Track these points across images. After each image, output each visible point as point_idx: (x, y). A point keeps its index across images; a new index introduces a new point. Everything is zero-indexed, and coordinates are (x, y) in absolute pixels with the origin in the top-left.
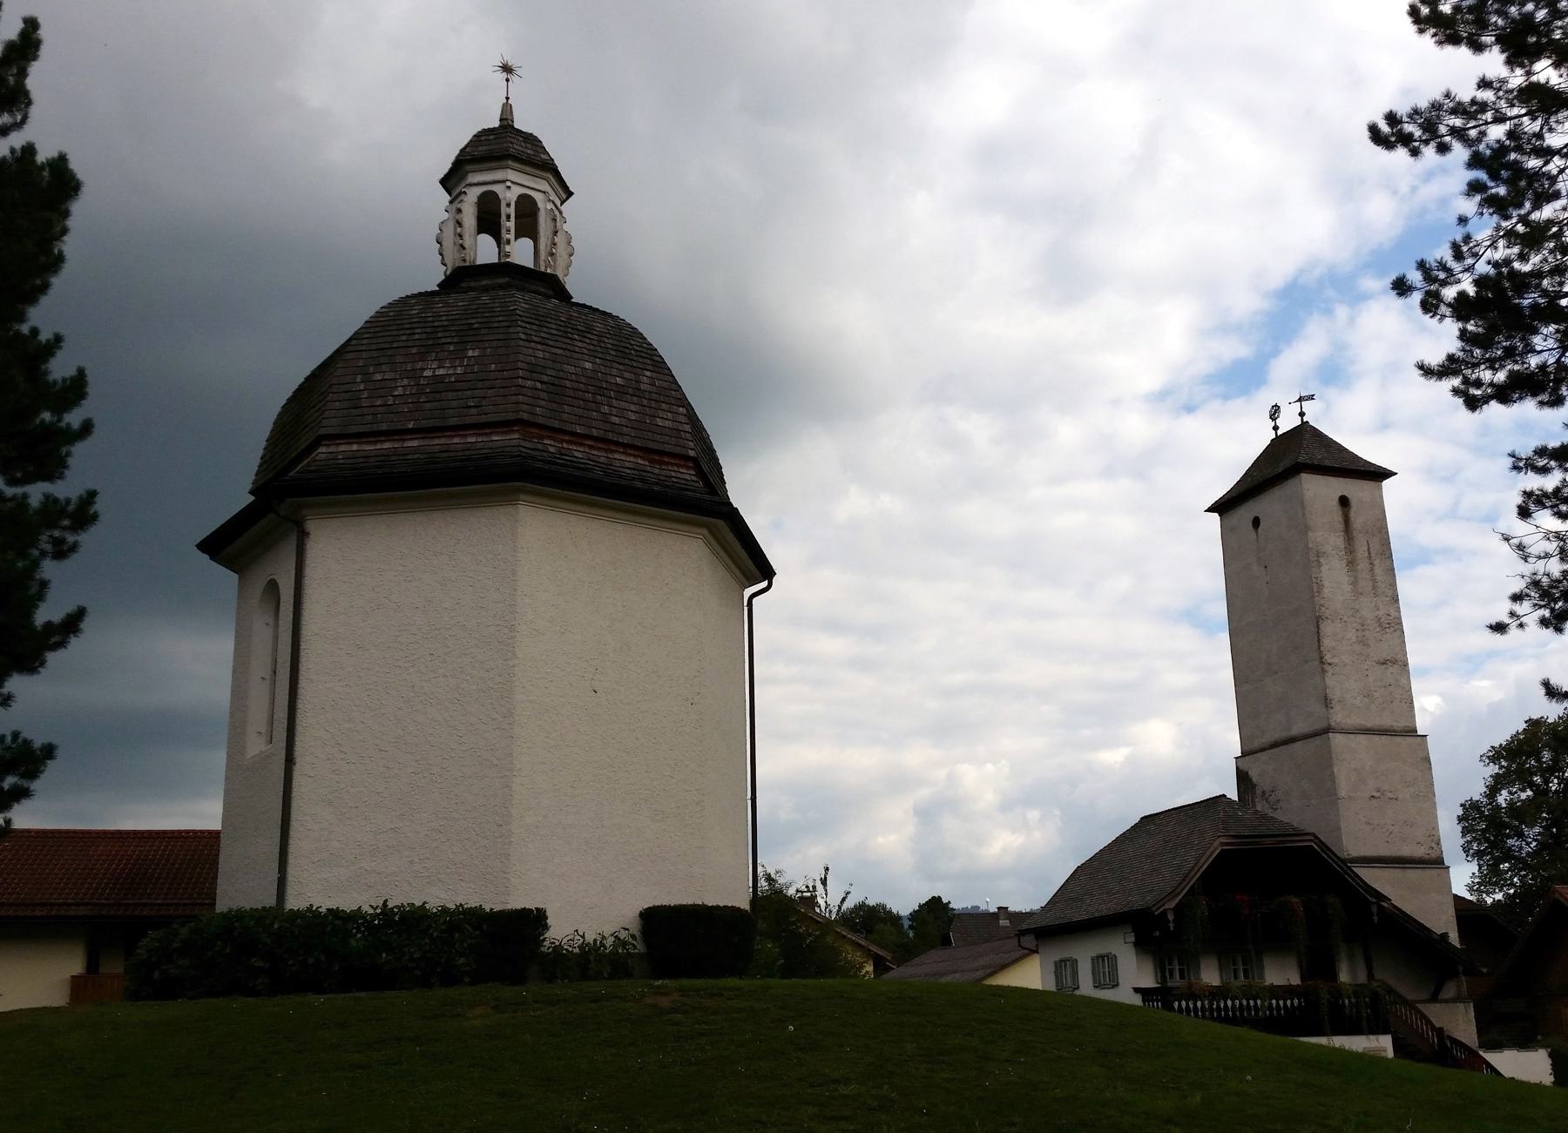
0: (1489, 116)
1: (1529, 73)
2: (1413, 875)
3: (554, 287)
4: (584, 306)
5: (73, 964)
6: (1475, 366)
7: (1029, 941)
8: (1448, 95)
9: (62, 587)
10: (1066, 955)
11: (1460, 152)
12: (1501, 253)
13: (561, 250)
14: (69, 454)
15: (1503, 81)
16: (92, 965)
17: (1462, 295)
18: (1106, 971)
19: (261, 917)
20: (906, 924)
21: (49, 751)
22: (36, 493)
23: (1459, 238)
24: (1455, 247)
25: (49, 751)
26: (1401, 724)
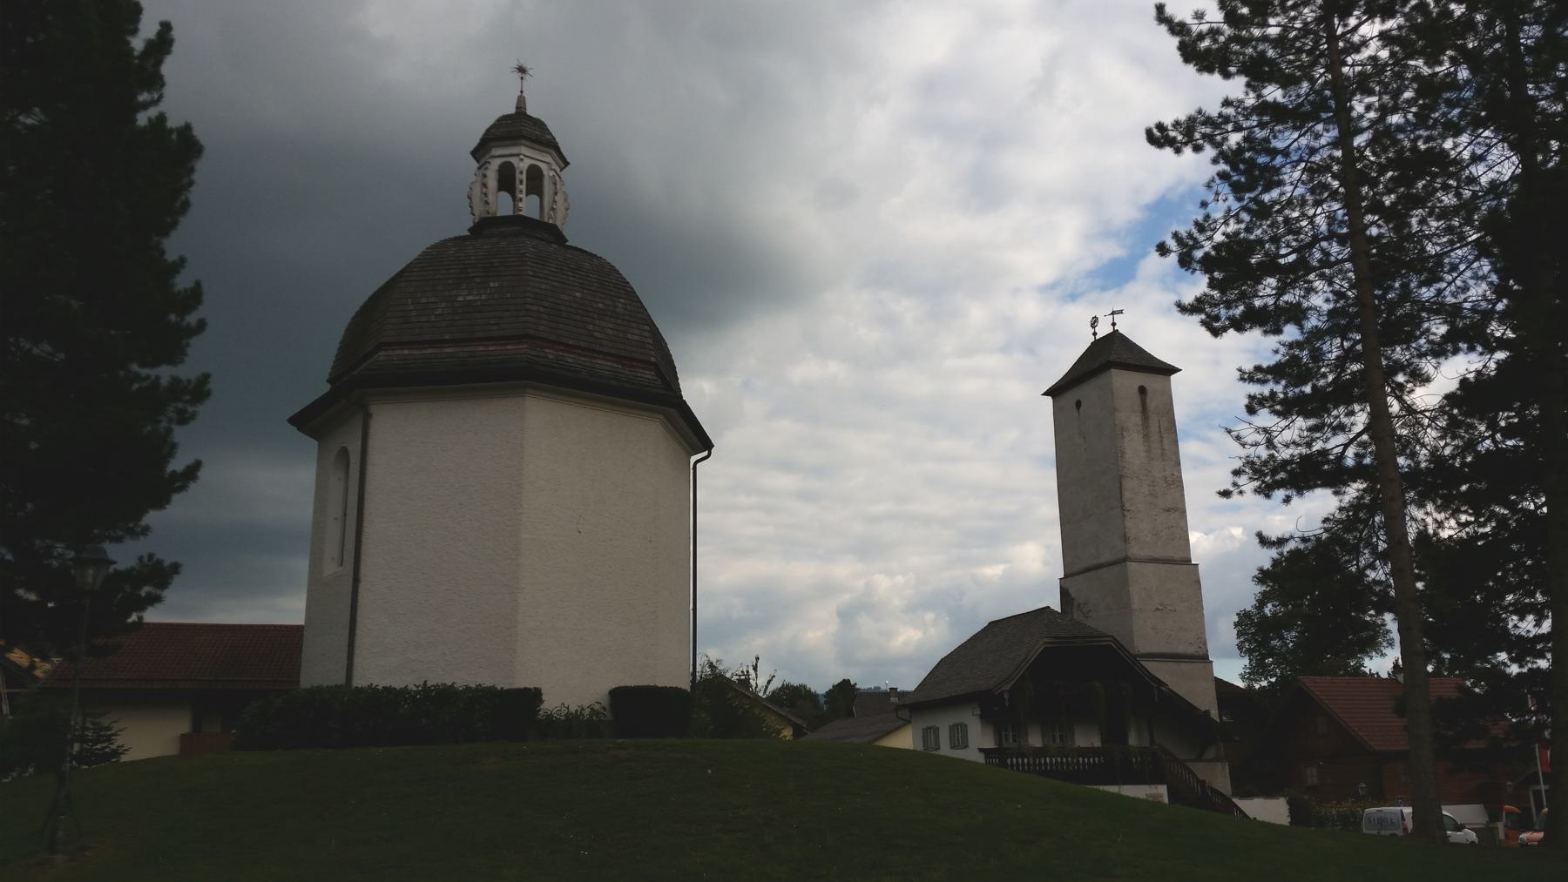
0: (1230, 127)
1: (1259, 96)
2: (1185, 667)
3: (554, 234)
4: (576, 249)
5: (183, 726)
6: (1216, 305)
7: (905, 714)
8: (1200, 112)
9: (188, 445)
10: (931, 724)
11: (1210, 152)
12: (1232, 227)
13: (560, 206)
14: (187, 345)
15: (1241, 102)
16: (197, 727)
17: (1207, 254)
18: (959, 737)
19: (335, 691)
20: (822, 700)
21: (175, 568)
22: (165, 373)
23: (1200, 218)
24: (1197, 224)
25: (175, 568)
26: (1178, 556)
